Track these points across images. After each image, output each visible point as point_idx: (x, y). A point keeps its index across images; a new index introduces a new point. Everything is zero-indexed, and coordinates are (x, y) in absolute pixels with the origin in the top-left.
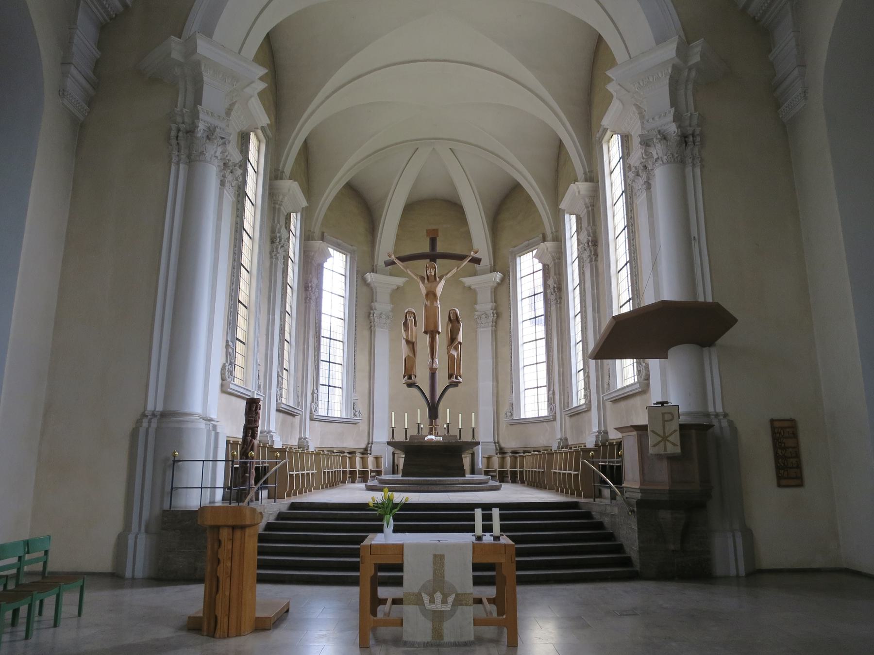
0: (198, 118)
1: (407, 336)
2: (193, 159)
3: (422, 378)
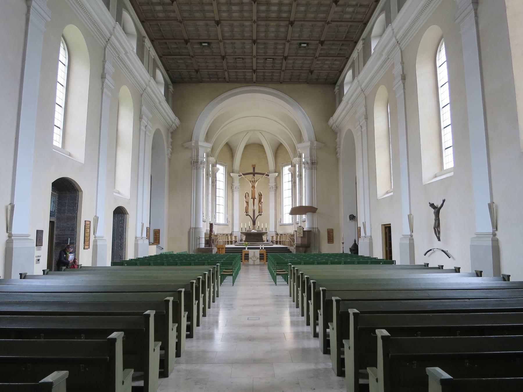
2: (197, 168)
3: (251, 213)
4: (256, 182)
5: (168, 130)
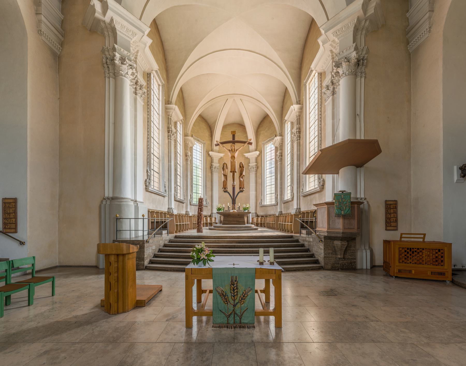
1: (224, 173)
3: (230, 189)
4: (236, 151)
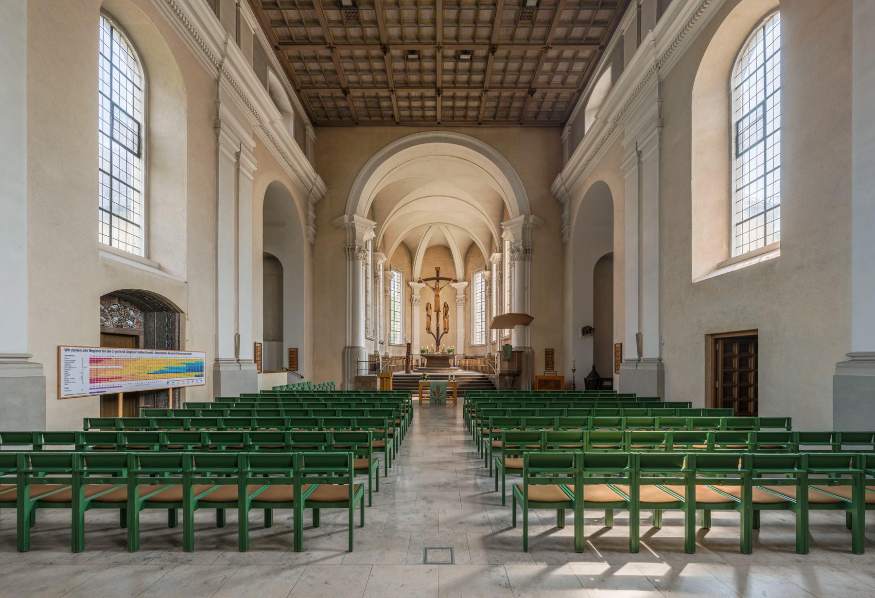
0: (355, 245)
2: (355, 259)
5: (307, 198)
